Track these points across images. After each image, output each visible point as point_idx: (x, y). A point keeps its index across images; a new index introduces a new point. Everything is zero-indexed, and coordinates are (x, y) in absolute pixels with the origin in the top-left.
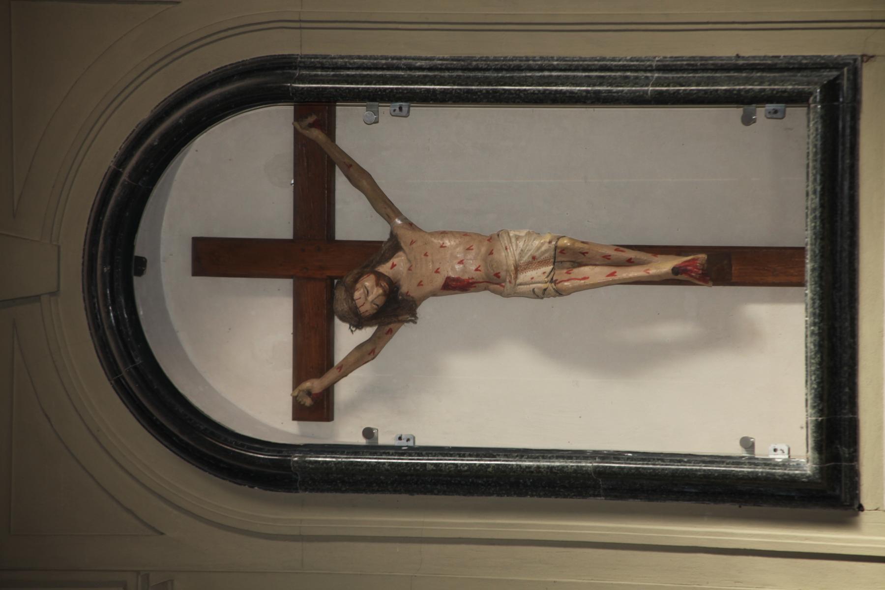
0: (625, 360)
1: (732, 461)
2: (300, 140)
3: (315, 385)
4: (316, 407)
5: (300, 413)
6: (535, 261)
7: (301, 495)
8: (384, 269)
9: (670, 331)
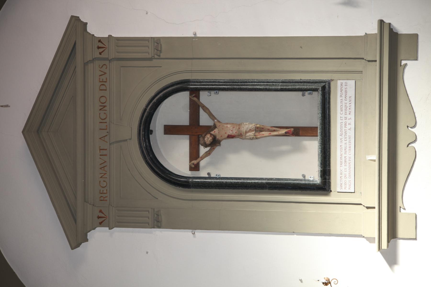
2: (191, 100)
3: (195, 162)
4: (195, 168)
5: (191, 169)
6: (250, 130)
7: (192, 189)
8: (212, 133)
9: (284, 148)
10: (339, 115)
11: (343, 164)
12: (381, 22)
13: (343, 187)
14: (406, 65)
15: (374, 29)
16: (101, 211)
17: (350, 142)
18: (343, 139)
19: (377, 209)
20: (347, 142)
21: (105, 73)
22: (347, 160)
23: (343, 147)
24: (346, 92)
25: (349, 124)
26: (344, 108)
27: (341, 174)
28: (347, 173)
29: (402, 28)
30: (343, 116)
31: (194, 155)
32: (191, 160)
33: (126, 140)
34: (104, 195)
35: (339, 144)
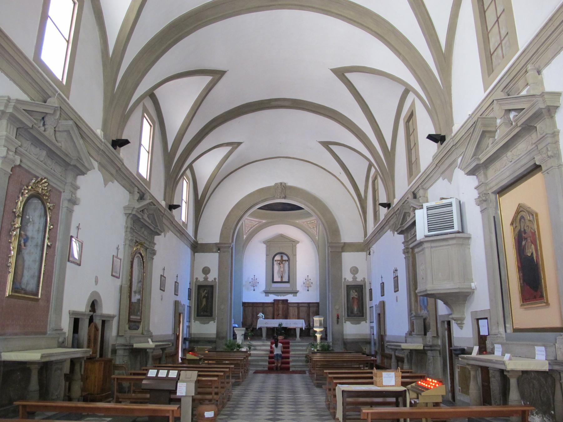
29: (298, 294)
31: (278, 261)
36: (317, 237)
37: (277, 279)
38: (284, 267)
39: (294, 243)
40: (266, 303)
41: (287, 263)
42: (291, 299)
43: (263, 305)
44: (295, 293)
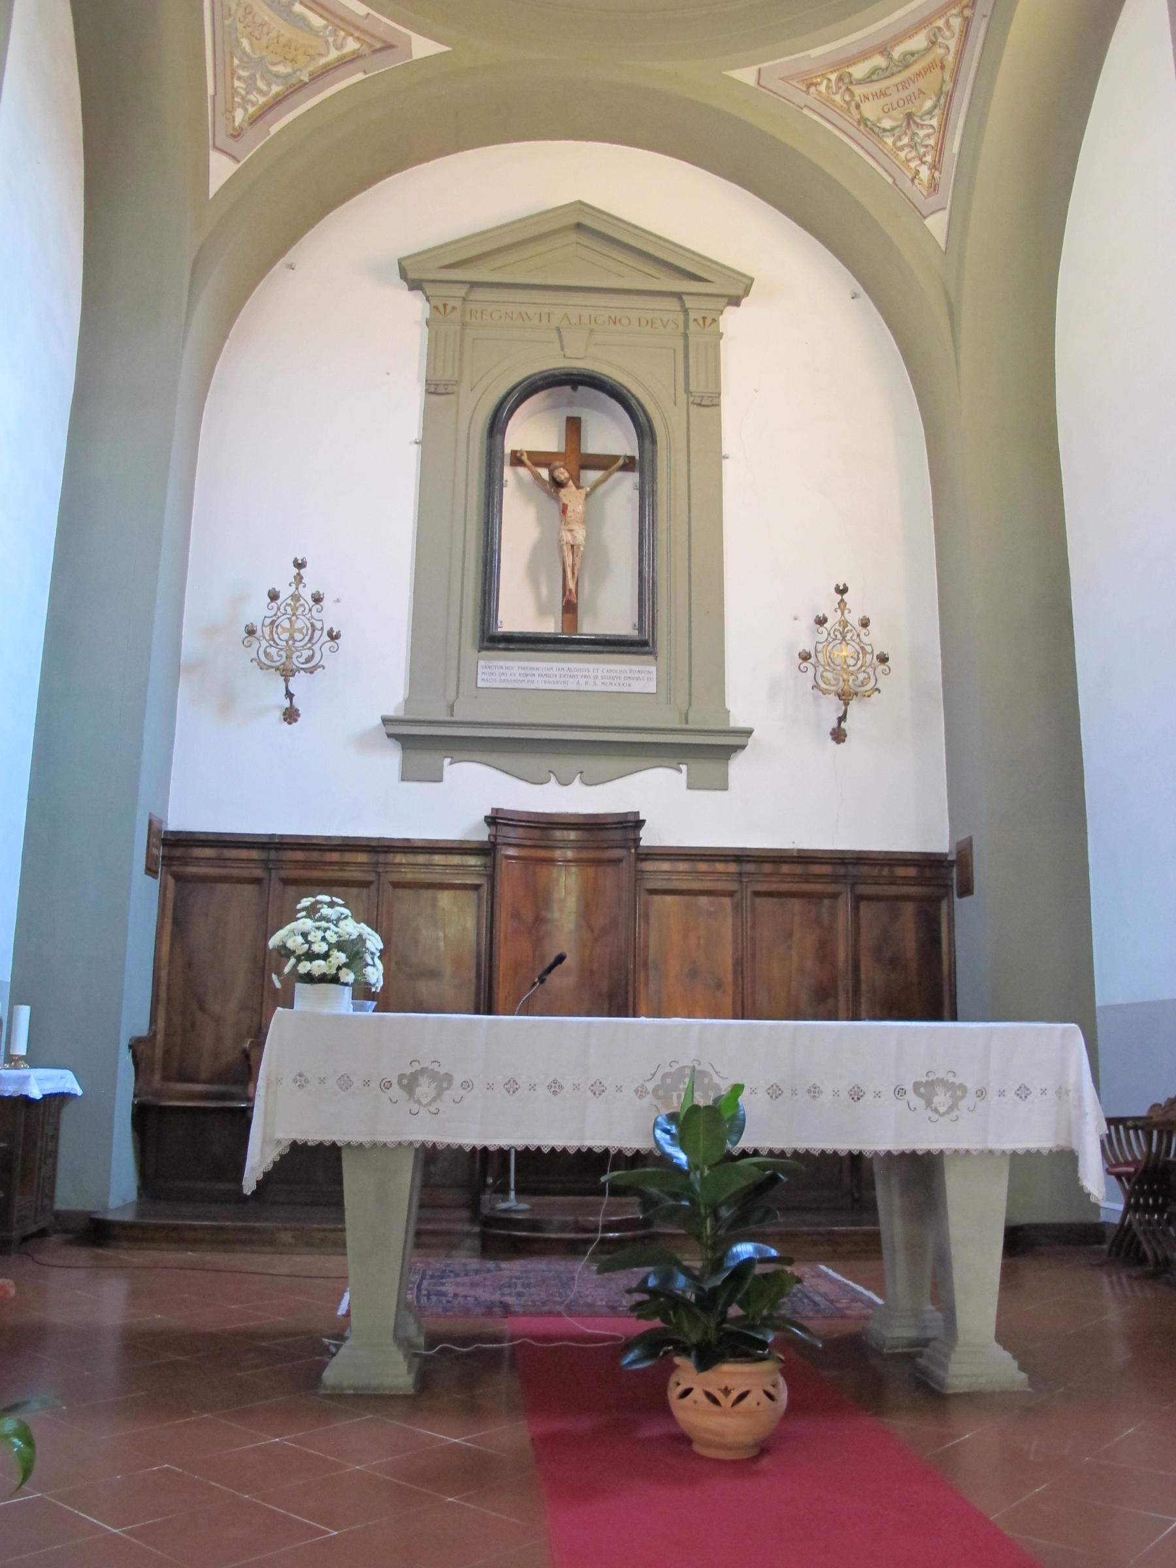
0: (533, 571)
1: (515, 395)
2: (617, 458)
3: (525, 458)
4: (517, 460)
5: (514, 453)
6: (574, 537)
7: (485, 442)
8: (571, 483)
9: (544, 591)
10: (600, 667)
11: (522, 672)
12: (748, 733)
13: (486, 671)
14: (680, 771)
15: (738, 721)
16: (454, 308)
17: (578, 670)
18: (562, 672)
19: (449, 719)
20: (558, 678)
21: (665, 327)
22: (529, 678)
23: (551, 672)
24: (638, 679)
25: (586, 683)
26: (612, 674)
27: (507, 668)
28: (508, 677)
29: (737, 767)
30: (600, 674)
31: (540, 459)
32: (530, 453)
33: (562, 349)
34: (479, 315)
35: (555, 665)
36: (937, 224)
37: (518, 611)
38: (591, 520)
39: (696, 291)
40: (409, 847)
41: (626, 486)
42: (672, 810)
43: (364, 869)
44: (709, 751)
